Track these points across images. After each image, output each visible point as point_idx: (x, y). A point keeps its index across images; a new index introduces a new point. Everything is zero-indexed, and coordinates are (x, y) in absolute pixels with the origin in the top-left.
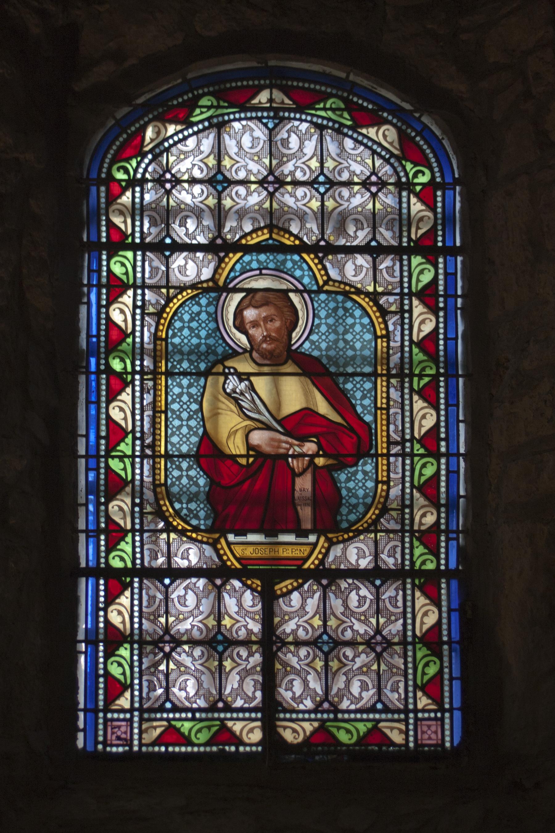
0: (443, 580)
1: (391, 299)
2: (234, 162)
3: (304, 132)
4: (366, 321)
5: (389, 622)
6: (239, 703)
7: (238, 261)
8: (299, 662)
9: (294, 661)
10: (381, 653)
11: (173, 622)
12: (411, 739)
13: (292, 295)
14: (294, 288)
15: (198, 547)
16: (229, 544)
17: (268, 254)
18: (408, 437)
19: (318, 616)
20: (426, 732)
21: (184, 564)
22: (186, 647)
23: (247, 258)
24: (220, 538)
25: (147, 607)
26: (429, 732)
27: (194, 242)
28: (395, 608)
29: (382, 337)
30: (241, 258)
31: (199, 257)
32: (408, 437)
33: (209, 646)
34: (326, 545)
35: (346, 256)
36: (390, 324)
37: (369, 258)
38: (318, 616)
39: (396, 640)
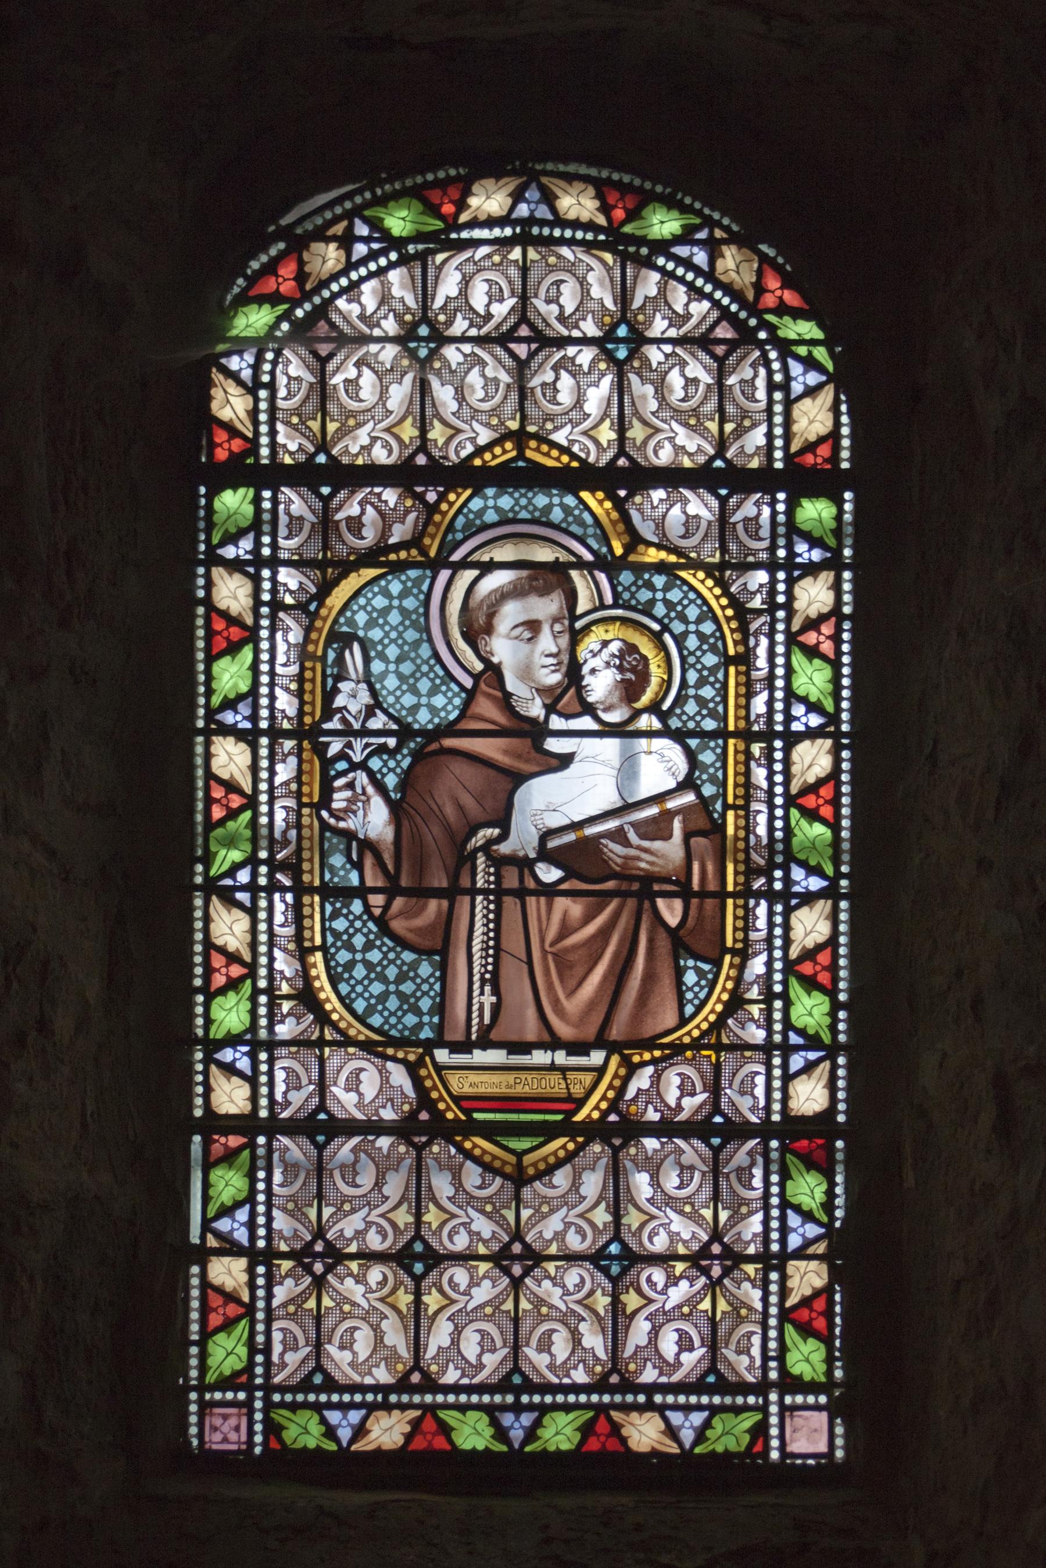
4: (708, 628)
6: (451, 1377)
8: (367, 1295)
9: (555, 1295)
10: (720, 1280)
13: (574, 574)
14: (574, 560)
22: (354, 1266)
25: (281, 1185)
28: (352, 1186)
33: (398, 1265)
34: (622, 1072)
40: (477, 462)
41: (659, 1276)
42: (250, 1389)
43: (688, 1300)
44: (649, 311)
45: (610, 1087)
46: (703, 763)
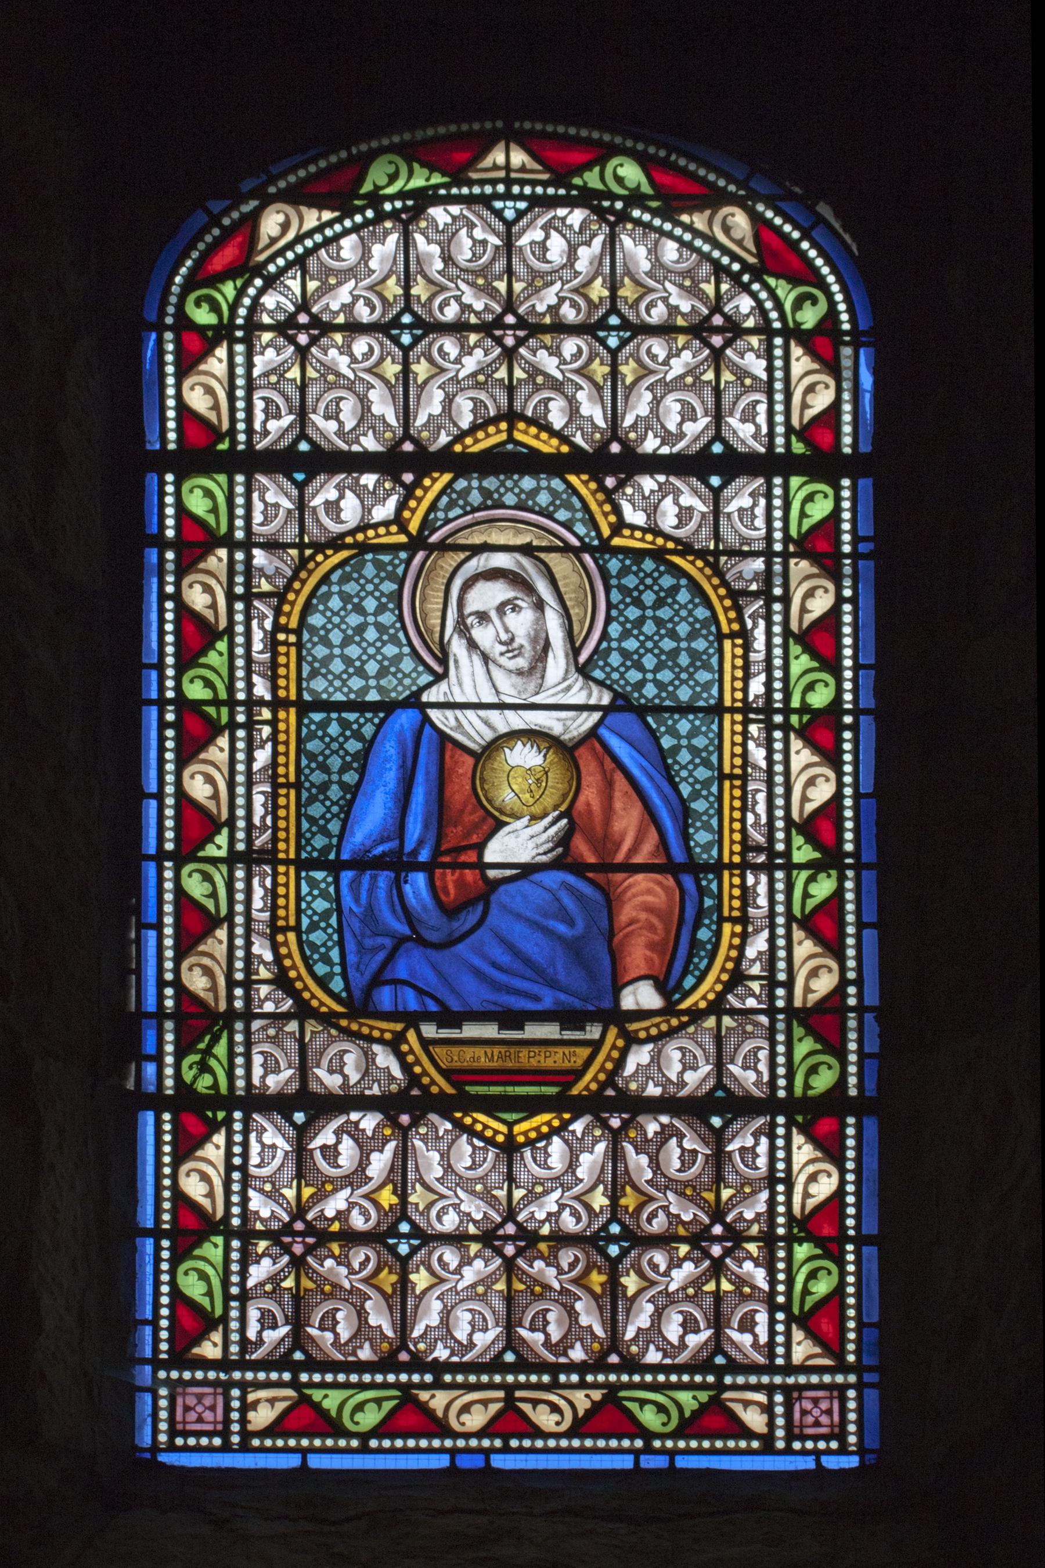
0: (172, 446)
1: (269, 1007)
2: (434, 289)
3: (577, 229)
4: (701, 613)
5: (279, 371)
7: (442, 492)
11: (705, 371)
12: (780, 1421)
15: (362, 1048)
16: (426, 1043)
17: (502, 477)
18: (241, 733)
19: (420, 382)
20: (810, 1412)
21: (333, 1082)
23: (461, 484)
24: (405, 1030)
26: (816, 1412)
27: (356, 448)
29: (732, 635)
30: (449, 485)
31: (656, 1085)
32: (241, 733)
35: (362, 1092)
36: (748, 612)
37: (314, 1086)
38: (420, 382)
39: (267, 337)
40: (458, 448)
41: (660, 1258)
42: (230, 1384)
43: (693, 1282)
44: (641, 430)
45: (608, 1058)
46: (695, 811)
